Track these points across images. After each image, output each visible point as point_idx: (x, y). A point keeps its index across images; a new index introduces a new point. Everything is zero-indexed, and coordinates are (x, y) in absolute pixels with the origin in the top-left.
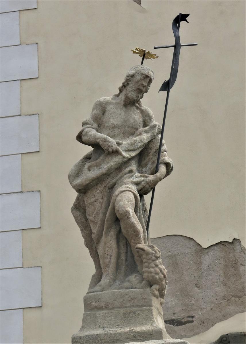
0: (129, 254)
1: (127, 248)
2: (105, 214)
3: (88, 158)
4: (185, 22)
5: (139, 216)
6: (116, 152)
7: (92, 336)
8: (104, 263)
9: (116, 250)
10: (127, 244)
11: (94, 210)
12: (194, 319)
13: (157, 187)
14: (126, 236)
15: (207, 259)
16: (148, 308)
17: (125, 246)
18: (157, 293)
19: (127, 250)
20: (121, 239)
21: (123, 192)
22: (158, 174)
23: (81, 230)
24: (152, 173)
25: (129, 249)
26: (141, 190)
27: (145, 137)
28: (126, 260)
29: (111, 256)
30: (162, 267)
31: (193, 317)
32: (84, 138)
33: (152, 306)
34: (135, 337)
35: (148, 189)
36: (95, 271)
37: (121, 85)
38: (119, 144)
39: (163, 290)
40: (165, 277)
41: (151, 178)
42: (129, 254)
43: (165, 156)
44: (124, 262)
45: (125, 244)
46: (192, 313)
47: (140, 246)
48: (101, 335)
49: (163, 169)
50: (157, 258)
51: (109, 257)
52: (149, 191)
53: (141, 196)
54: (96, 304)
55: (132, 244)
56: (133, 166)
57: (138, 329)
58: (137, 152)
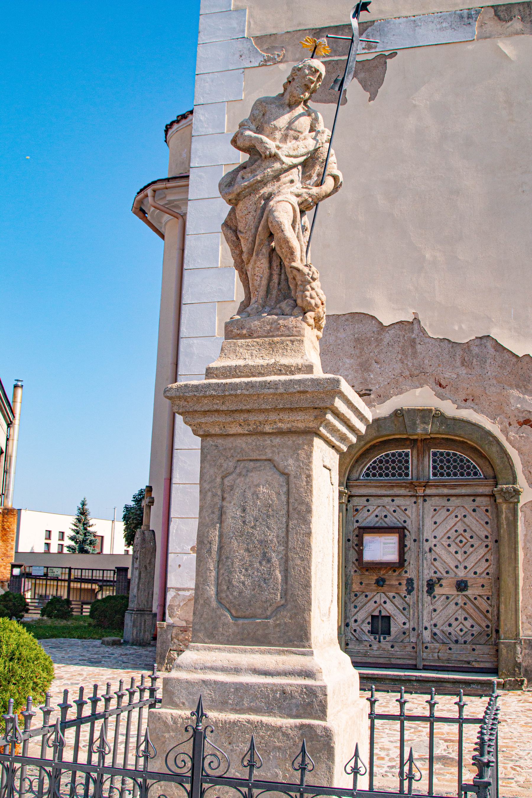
0: (275, 264)
1: (281, 269)
2: (257, 228)
3: (243, 167)
4: (365, 12)
5: (298, 233)
6: (275, 157)
7: (230, 367)
8: (253, 286)
9: (268, 270)
10: (280, 264)
11: (246, 224)
12: (371, 392)
13: (321, 204)
14: (281, 255)
15: (387, 337)
16: (298, 338)
17: (279, 267)
18: (311, 321)
19: (281, 271)
20: (274, 258)
21: (279, 202)
22: (324, 187)
23: (232, 250)
24: (317, 186)
25: (283, 271)
26: (302, 203)
27: (311, 145)
28: (279, 284)
29: (261, 278)
30: (320, 292)
31: (370, 390)
32: (239, 143)
33: (304, 336)
34: (280, 370)
35: (310, 204)
36: (244, 298)
37: (286, 81)
38: (278, 148)
39: (319, 321)
40: (322, 304)
41: (315, 190)
42: (283, 276)
43: (333, 168)
44: (276, 285)
45: (279, 264)
46: (370, 387)
47: (294, 264)
48: (240, 366)
49: (329, 183)
50: (314, 279)
51: (259, 279)
52: (312, 207)
53: (302, 212)
54: (238, 332)
55: (286, 263)
56: (295, 174)
57: (285, 361)
58: (302, 159)
